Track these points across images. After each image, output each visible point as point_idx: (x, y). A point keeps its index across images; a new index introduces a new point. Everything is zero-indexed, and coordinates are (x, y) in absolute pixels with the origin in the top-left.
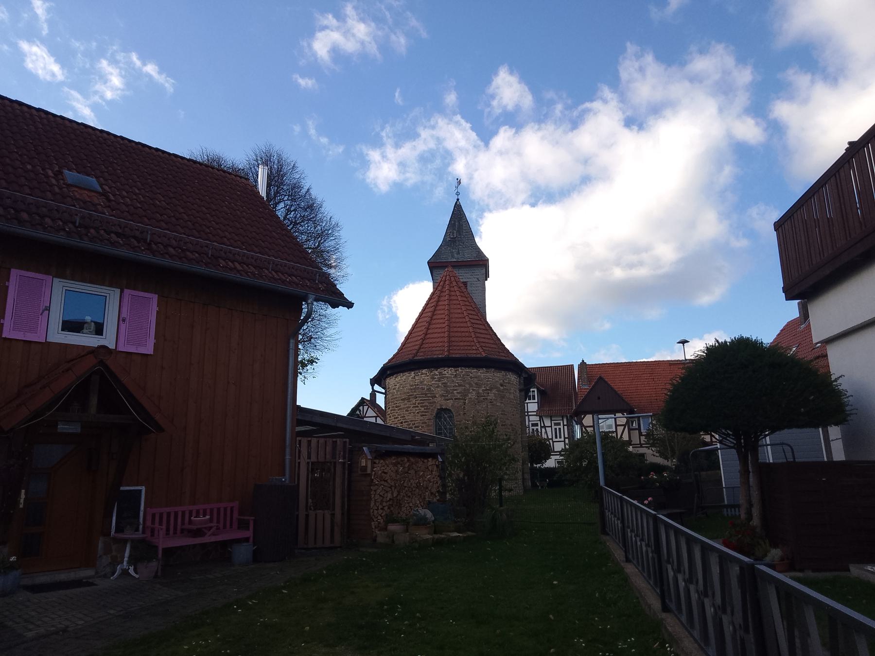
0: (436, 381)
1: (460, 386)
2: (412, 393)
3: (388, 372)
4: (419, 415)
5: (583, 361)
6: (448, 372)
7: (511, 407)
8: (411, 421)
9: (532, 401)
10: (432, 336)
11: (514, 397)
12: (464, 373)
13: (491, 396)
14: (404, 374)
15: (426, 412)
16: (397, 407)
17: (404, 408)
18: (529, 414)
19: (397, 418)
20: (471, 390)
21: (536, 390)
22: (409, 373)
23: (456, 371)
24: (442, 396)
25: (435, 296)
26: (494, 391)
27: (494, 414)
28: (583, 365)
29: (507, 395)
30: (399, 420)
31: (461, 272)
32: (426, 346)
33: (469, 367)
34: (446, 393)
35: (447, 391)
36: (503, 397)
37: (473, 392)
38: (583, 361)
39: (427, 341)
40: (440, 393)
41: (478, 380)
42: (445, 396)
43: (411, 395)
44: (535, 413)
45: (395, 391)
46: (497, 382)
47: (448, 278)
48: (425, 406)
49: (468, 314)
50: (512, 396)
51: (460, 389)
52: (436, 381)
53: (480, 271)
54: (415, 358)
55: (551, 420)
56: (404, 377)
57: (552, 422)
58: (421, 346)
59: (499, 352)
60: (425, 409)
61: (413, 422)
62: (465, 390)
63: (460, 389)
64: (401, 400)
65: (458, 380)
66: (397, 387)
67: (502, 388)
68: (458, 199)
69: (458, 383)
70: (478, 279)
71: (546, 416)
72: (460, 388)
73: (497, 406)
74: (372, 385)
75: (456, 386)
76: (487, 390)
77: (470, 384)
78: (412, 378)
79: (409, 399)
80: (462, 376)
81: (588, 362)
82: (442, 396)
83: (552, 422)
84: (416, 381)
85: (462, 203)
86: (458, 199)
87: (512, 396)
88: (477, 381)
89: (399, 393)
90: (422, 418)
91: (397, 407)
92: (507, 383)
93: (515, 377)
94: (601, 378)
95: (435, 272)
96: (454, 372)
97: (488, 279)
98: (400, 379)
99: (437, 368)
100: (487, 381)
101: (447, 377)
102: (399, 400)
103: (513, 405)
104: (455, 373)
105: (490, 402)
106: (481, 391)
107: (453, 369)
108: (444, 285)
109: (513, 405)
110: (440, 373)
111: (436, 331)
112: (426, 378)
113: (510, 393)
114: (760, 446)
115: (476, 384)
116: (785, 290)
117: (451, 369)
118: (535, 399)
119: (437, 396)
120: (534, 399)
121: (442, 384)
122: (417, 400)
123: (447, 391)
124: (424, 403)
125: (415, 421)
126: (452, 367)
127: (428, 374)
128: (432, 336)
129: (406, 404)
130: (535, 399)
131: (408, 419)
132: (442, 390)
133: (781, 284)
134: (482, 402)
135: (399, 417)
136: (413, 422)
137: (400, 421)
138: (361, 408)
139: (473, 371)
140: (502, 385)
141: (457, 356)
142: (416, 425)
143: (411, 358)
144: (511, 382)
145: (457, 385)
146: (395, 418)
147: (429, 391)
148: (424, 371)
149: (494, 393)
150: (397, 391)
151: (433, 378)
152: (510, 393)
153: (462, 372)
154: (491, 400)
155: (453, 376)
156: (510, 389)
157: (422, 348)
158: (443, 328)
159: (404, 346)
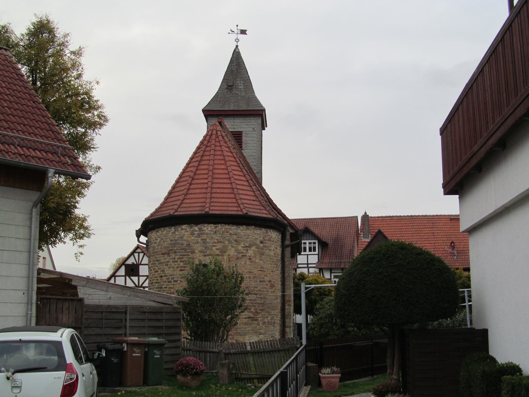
0: (196, 237)
1: (219, 242)
2: (171, 248)
3: (150, 226)
4: (178, 270)
5: (365, 213)
6: (208, 228)
7: (270, 264)
8: (171, 275)
9: (312, 253)
10: (193, 191)
11: (275, 254)
12: (223, 230)
13: (250, 253)
14: (165, 228)
15: (185, 267)
16: (157, 261)
17: (164, 262)
18: (306, 266)
19: (157, 271)
20: (230, 247)
21: (317, 242)
22: (170, 228)
23: (216, 227)
24: (201, 252)
25: (197, 155)
26: (253, 248)
27: (252, 271)
28: (365, 217)
29: (267, 252)
30: (159, 274)
31: (237, 121)
32: (188, 201)
33: (229, 224)
34: (205, 249)
35: (206, 248)
36: (262, 254)
37: (232, 249)
38: (365, 213)
39: (189, 196)
40: (200, 249)
41: (237, 237)
42: (204, 252)
43: (171, 250)
44: (314, 265)
45: (156, 245)
46: (256, 239)
47: (214, 132)
48: (184, 261)
49: (232, 170)
50: (272, 253)
51: (219, 246)
52: (196, 237)
53: (256, 122)
54: (176, 214)
55: (331, 273)
56: (165, 232)
57: (332, 274)
58: (183, 201)
59: (260, 209)
60: (184, 264)
61: (172, 277)
62: (224, 246)
63: (219, 246)
64: (162, 254)
65: (217, 237)
66: (158, 241)
67: (261, 245)
68: (237, 46)
69: (217, 239)
70: (253, 129)
71: (327, 269)
72: (220, 244)
73: (256, 262)
74: (138, 236)
75: (215, 243)
76: (246, 247)
77: (230, 242)
78: (172, 233)
79: (169, 253)
80: (221, 232)
81: (371, 214)
82: (201, 252)
83: (332, 274)
84: (176, 236)
85: (241, 50)
86: (237, 46)
87: (272, 253)
88: (236, 238)
89: (159, 247)
90: (181, 273)
91: (157, 261)
92: (267, 240)
93: (276, 235)
94: (380, 232)
95: (209, 119)
96: (214, 229)
97: (266, 128)
98: (161, 233)
99: (197, 224)
100: (247, 238)
101: (207, 234)
102: (159, 254)
103: (273, 262)
104: (215, 230)
105: (249, 259)
106: (240, 248)
107: (213, 225)
108: (209, 139)
109: (273, 262)
110: (200, 229)
111: (199, 186)
112: (186, 233)
113: (270, 250)
114: (288, 327)
115: (236, 241)
116: (444, 186)
117: (211, 225)
118: (315, 251)
119: (196, 252)
120: (314, 250)
121: (202, 240)
122: (176, 255)
123: (206, 248)
124: (183, 258)
125: (174, 275)
126: (212, 223)
127: (188, 230)
128: (193, 191)
129: (166, 259)
130: (315, 251)
131: (168, 273)
132: (201, 246)
133: (441, 181)
134: (240, 258)
135: (159, 271)
136: (172, 277)
137: (160, 275)
138: (136, 255)
139: (233, 228)
140: (261, 242)
141: (218, 212)
142: (175, 279)
143: (171, 213)
144: (272, 240)
145: (216, 241)
146: (155, 272)
147: (189, 247)
148: (184, 227)
149: (253, 250)
150: (158, 246)
151: (192, 234)
152: (270, 250)
153: (222, 229)
154: (250, 256)
155: (212, 232)
156: (271, 246)
157: (184, 203)
158: (206, 183)
159: (166, 200)
